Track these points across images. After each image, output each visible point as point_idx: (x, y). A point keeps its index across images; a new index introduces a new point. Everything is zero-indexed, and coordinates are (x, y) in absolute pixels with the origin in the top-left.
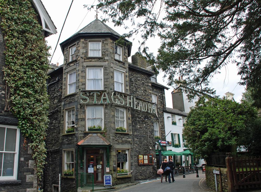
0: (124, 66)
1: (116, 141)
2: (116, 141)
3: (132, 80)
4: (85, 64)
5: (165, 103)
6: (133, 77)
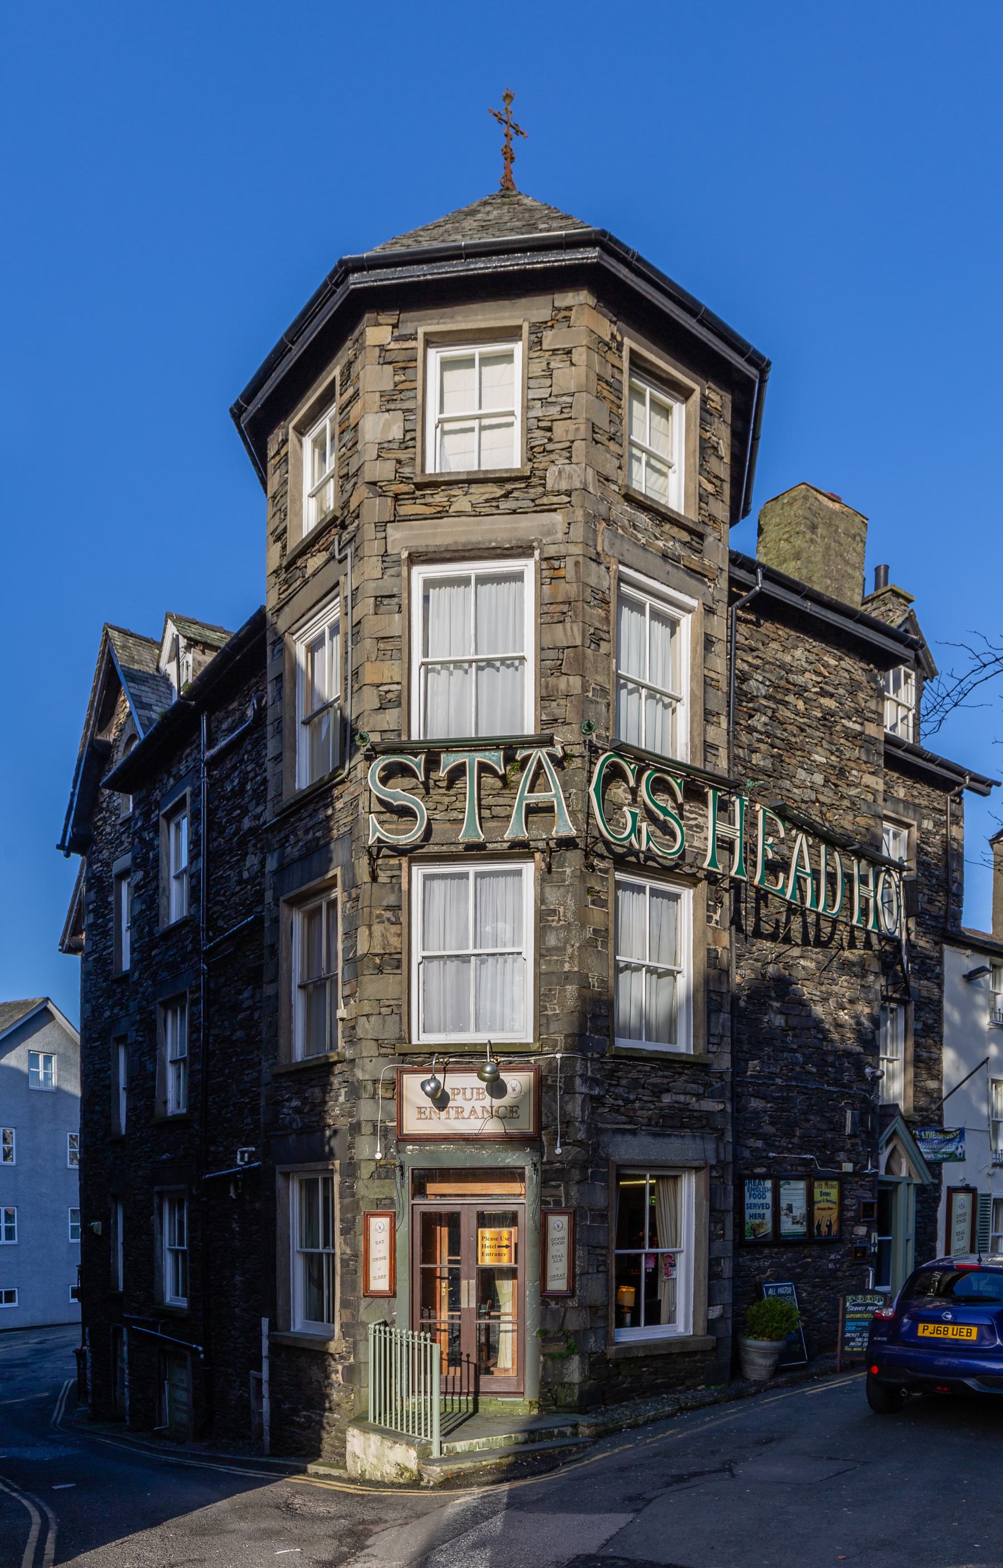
0: (694, 560)
1: (617, 1111)
2: (616, 1110)
3: (752, 685)
4: (401, 538)
5: (961, 885)
6: (757, 667)
